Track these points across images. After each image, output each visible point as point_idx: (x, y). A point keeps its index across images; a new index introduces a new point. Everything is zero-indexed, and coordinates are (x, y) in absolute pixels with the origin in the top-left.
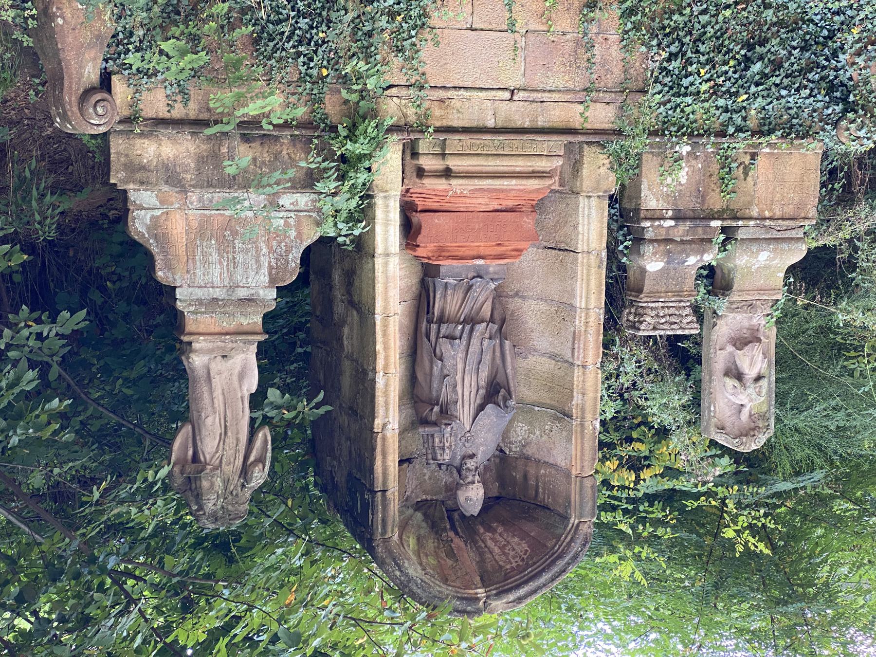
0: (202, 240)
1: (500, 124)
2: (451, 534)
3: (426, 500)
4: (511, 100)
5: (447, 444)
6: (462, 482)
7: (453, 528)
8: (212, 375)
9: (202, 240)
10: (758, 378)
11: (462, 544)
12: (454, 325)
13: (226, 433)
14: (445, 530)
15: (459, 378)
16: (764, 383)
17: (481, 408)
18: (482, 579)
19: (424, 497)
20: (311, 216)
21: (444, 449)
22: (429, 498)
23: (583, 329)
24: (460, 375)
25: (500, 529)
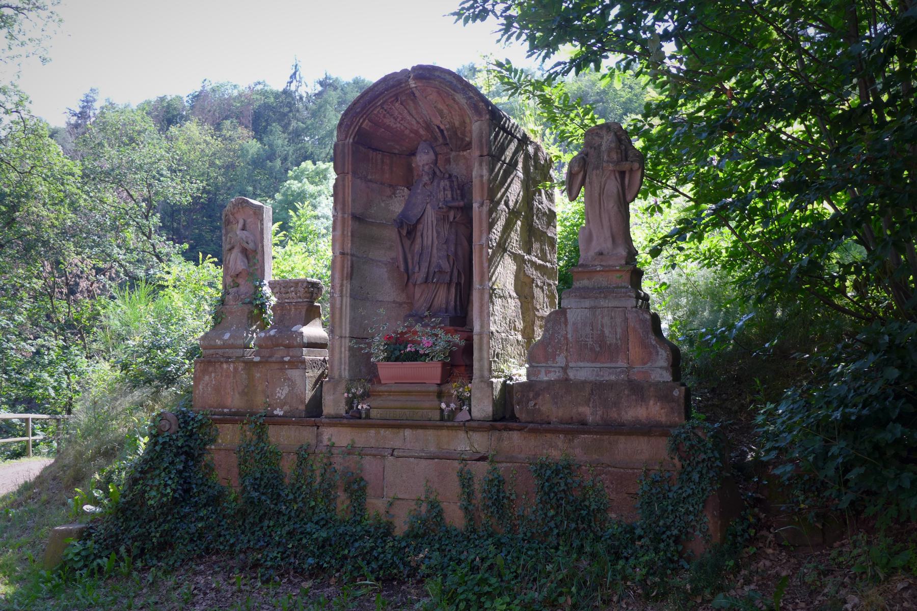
0: (616, 344)
1: (401, 431)
2: (442, 127)
3: (463, 151)
4: (393, 450)
5: (442, 193)
7: (442, 131)
8: (611, 239)
9: (616, 344)
10: (231, 249)
11: (433, 119)
13: (600, 196)
14: (448, 130)
15: (436, 242)
16: (228, 247)
17: (418, 221)
18: (414, 94)
19: (465, 153)
20: (537, 363)
21: (444, 189)
22: (461, 153)
23: (345, 282)
24: (435, 245)
25: (407, 132)
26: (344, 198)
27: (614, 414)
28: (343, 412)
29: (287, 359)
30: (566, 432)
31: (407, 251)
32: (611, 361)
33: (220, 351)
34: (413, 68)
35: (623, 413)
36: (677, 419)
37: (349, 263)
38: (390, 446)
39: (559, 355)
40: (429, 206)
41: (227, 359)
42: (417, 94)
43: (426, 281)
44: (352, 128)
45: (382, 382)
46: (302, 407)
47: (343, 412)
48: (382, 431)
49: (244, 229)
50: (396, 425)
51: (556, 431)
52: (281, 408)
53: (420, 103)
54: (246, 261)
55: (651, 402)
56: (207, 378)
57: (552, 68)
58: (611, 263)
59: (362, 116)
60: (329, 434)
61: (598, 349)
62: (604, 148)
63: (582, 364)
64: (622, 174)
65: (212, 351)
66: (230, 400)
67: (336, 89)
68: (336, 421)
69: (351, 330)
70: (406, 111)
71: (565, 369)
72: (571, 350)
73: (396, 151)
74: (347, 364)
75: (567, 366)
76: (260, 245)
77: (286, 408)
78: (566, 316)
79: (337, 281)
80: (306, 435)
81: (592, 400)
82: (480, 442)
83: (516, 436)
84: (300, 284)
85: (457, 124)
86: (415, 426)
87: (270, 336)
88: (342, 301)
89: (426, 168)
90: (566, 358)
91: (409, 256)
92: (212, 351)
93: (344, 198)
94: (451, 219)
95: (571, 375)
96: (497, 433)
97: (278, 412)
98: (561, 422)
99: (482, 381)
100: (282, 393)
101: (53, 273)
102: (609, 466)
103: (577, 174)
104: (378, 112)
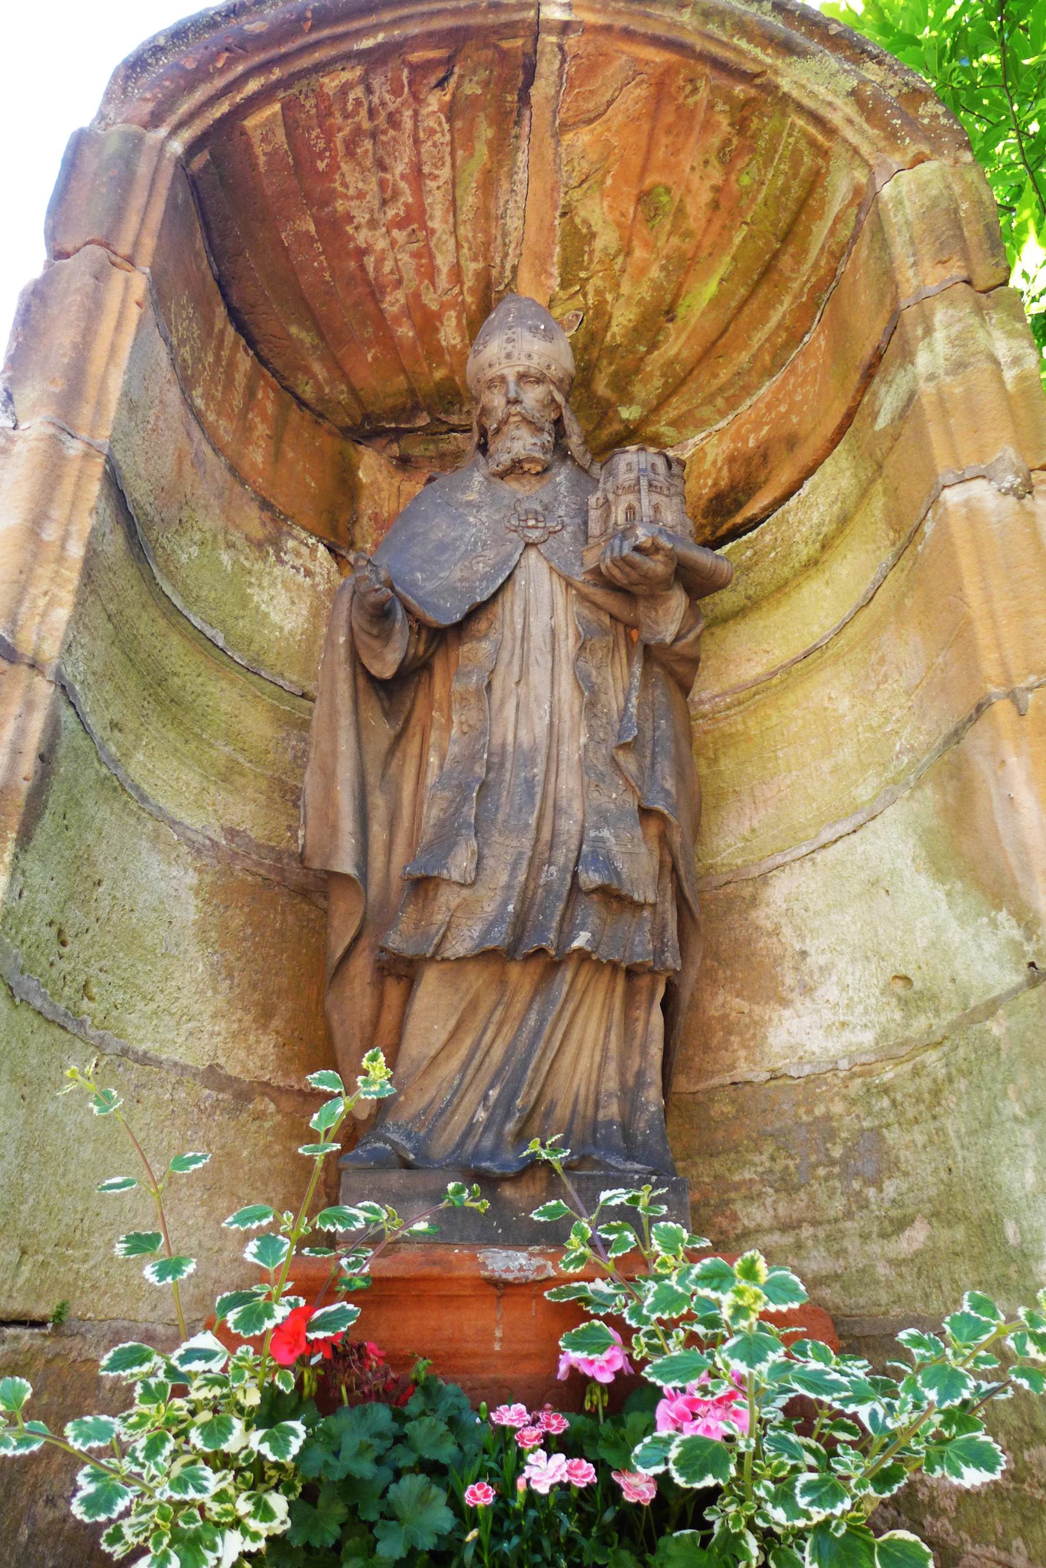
6: (559, 398)
11: (525, 276)
12: (604, 953)
26: (83, 350)
31: (372, 779)
44: (200, 94)
53: (522, 158)
57: (408, 610)
59: (264, 67)
70: (445, 173)
73: (307, 392)
89: (533, 396)
93: (83, 350)
104: (344, 89)
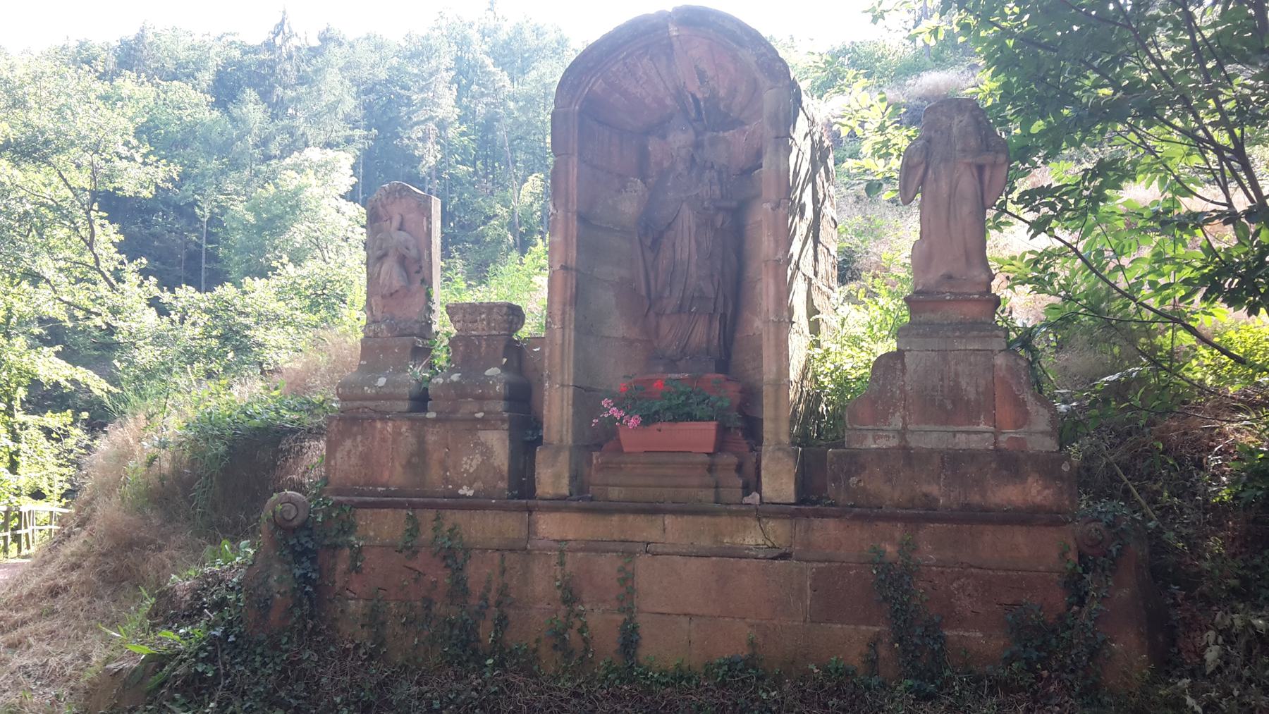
1: (658, 519)
2: (699, 96)
3: (724, 131)
7: (696, 101)
14: (706, 100)
21: (710, 181)
22: (721, 134)
27: (975, 498)
28: (565, 491)
29: (480, 415)
30: (907, 520)
32: (970, 423)
33: (371, 404)
34: (677, 11)
35: (989, 493)
36: (1067, 502)
37: (574, 281)
38: (642, 539)
39: (893, 414)
40: (684, 206)
41: (383, 416)
42: (676, 45)
43: (680, 309)
45: (625, 450)
46: (502, 485)
47: (565, 491)
48: (631, 518)
49: (401, 228)
50: (652, 509)
51: (891, 518)
52: (470, 486)
54: (404, 274)
55: (1030, 480)
56: (348, 443)
58: (965, 290)
60: (549, 526)
61: (949, 407)
62: (955, 130)
63: (927, 427)
64: (981, 168)
65: (357, 404)
66: (386, 475)
67: (340, 44)
68: (557, 504)
69: (575, 379)
71: (902, 433)
72: (911, 407)
74: (570, 424)
75: (904, 428)
76: (426, 253)
77: (479, 485)
78: (903, 360)
79: (557, 308)
80: (508, 525)
81: (943, 476)
82: (778, 531)
83: (831, 524)
84: (495, 310)
85: (722, 93)
86: (680, 510)
87: (452, 382)
88: (563, 335)
89: (683, 152)
90: (903, 418)
91: (652, 275)
92: (357, 404)
94: (719, 224)
95: (913, 442)
96: (804, 522)
97: (465, 491)
98: (898, 506)
99: (779, 449)
100: (470, 463)
101: (470, 285)
102: (971, 566)
103: (916, 166)
